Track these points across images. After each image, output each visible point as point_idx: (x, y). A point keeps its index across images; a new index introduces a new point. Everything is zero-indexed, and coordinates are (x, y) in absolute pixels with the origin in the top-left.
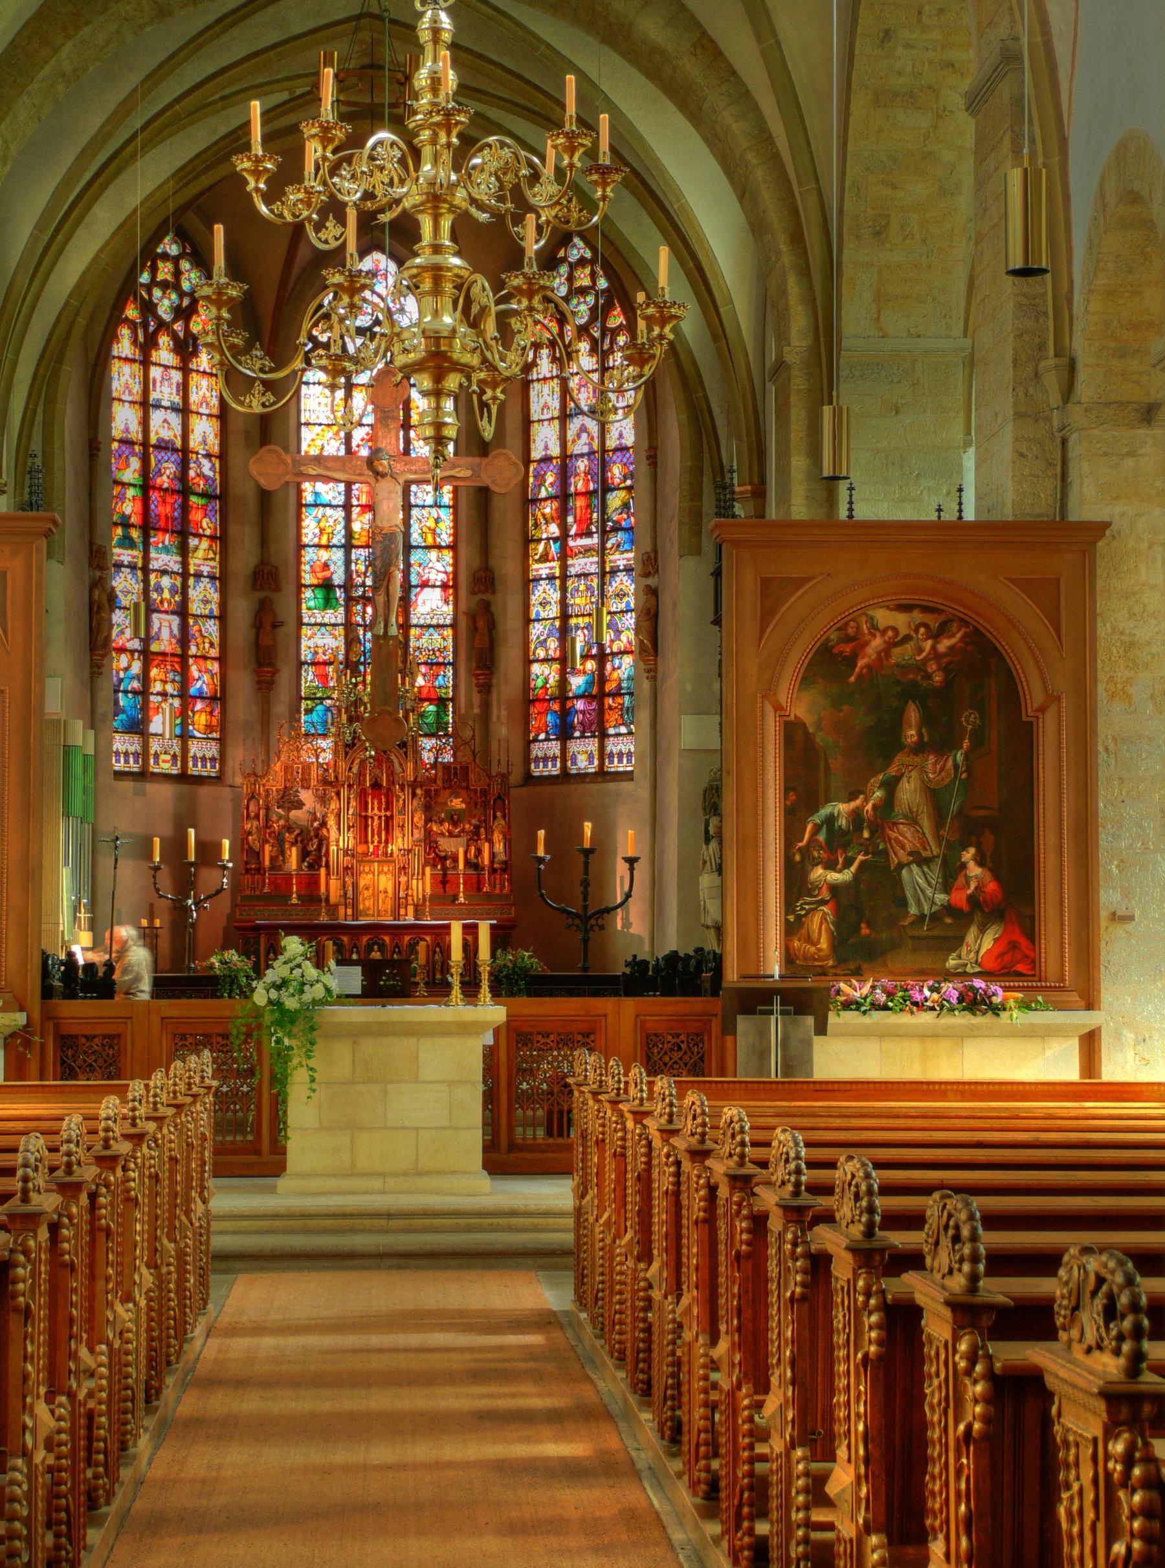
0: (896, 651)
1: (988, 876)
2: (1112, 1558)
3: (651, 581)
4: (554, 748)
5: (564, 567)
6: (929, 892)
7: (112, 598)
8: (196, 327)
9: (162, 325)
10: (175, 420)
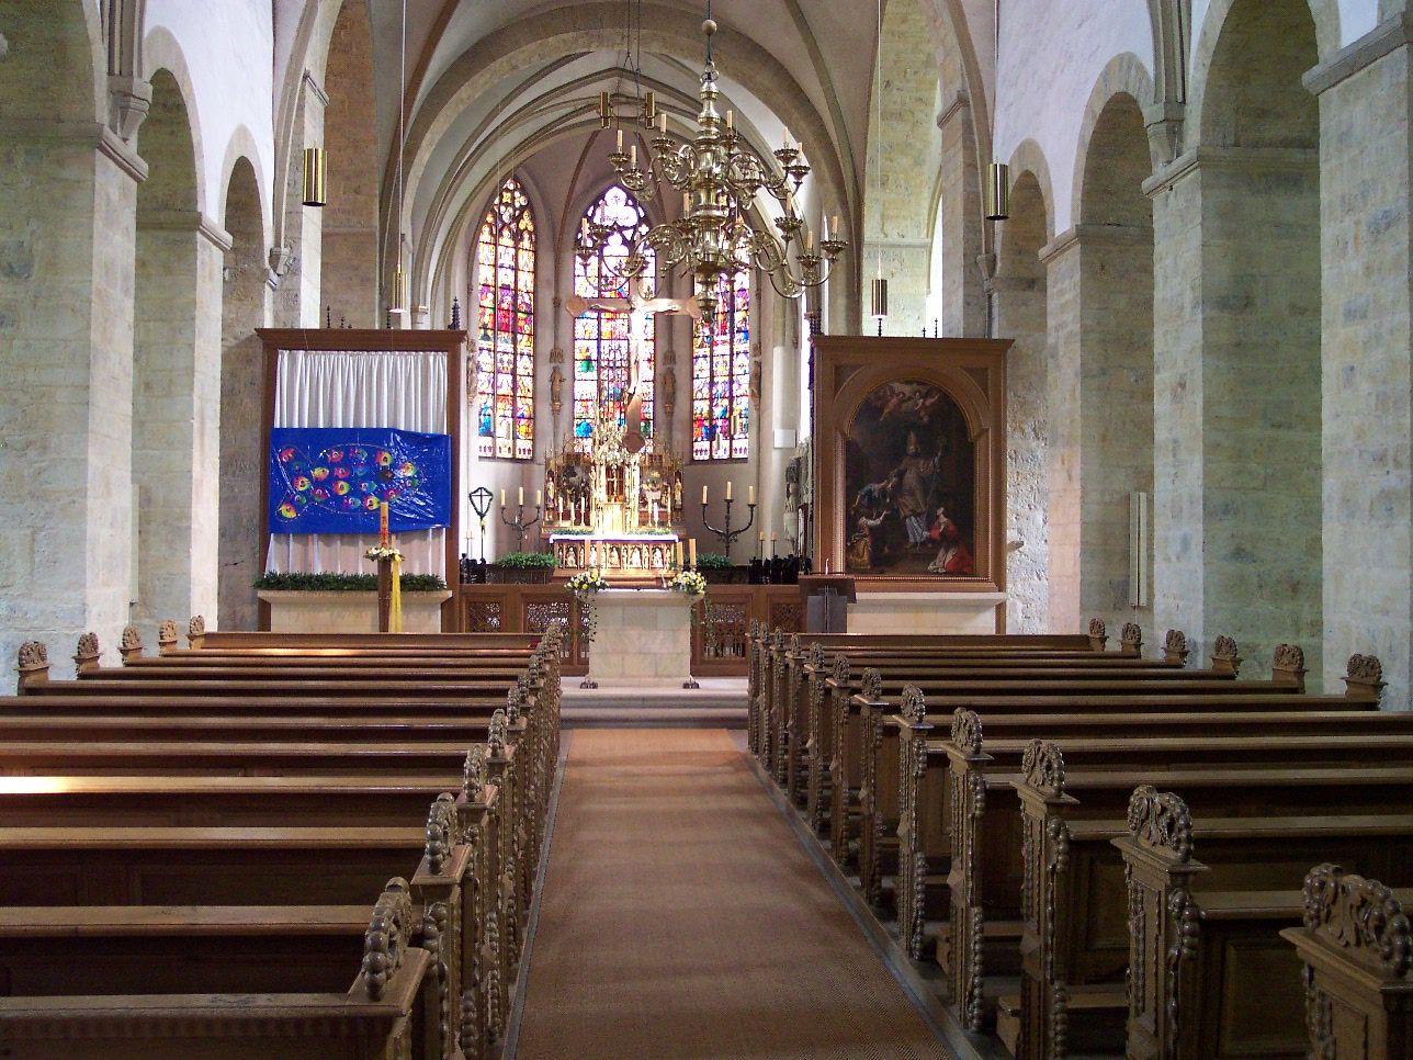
0: (904, 406)
1: (950, 523)
2: (1169, 955)
3: (757, 359)
4: (706, 445)
5: (712, 351)
6: (920, 530)
7: (478, 368)
8: (522, 226)
9: (504, 224)
10: (511, 274)
